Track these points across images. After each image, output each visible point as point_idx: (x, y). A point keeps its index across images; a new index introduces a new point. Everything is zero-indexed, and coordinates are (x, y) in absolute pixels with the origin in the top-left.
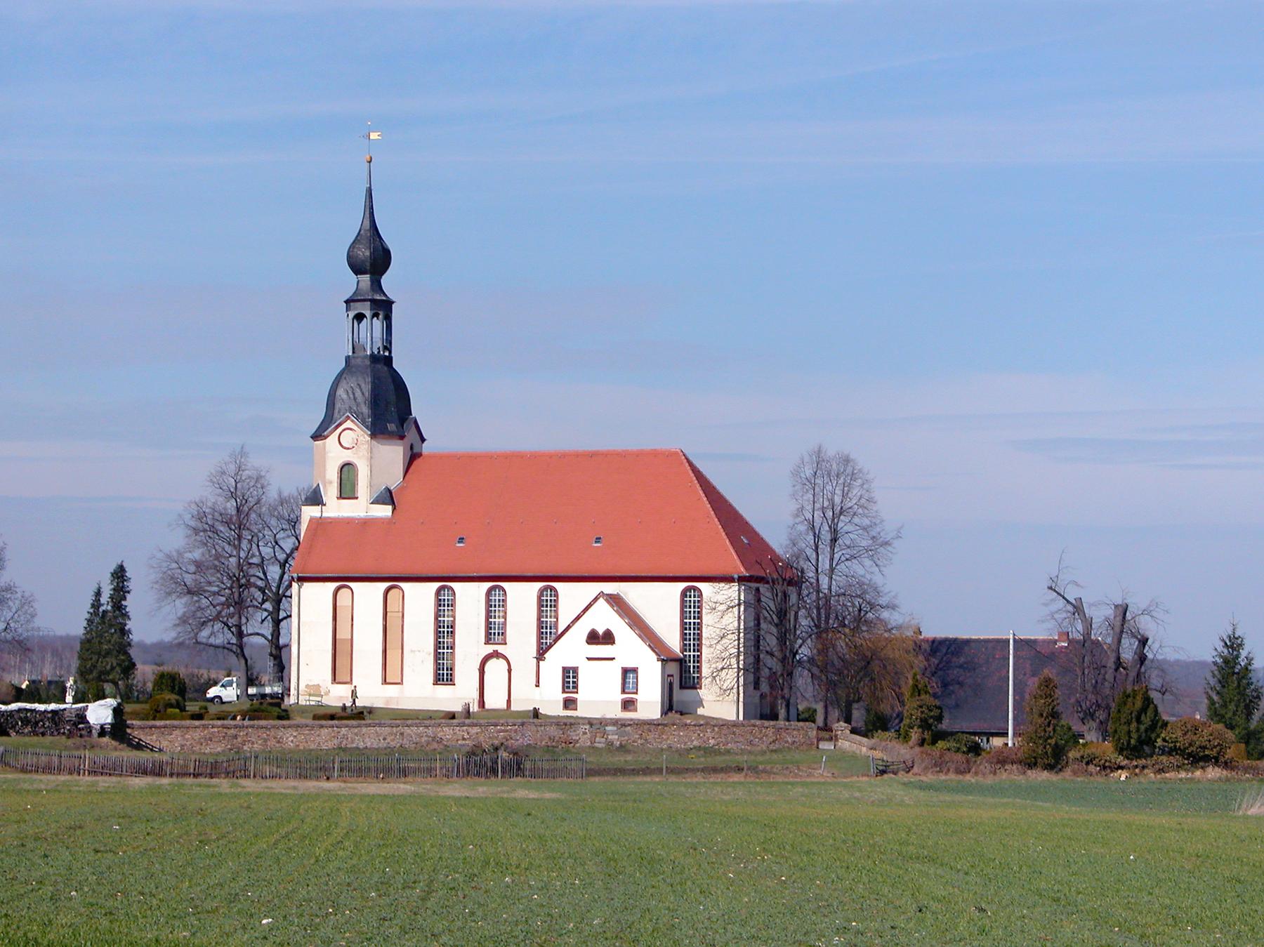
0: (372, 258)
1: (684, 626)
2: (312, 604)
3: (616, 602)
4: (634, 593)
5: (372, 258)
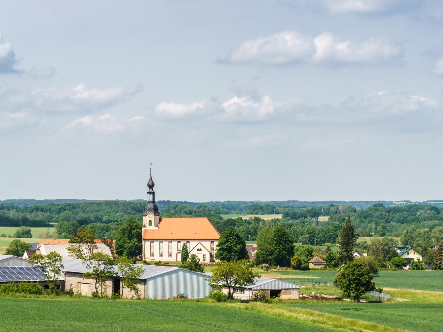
0: (151, 186)
2: (146, 246)
4: (203, 243)
5: (151, 186)
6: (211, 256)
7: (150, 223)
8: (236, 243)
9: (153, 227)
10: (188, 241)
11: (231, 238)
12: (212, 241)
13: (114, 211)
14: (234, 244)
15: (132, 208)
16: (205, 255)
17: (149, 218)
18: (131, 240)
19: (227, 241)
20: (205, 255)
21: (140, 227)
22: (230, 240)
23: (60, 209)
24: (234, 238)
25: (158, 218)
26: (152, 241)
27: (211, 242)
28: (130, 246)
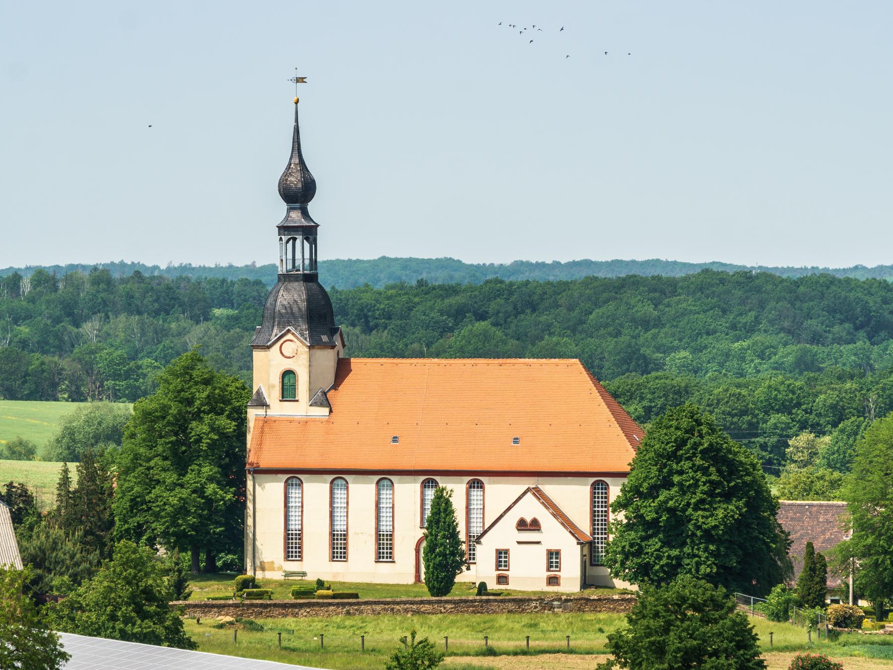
0: (299, 192)
1: (593, 514)
2: (266, 500)
3: (538, 493)
4: (551, 489)
5: (299, 192)
6: (591, 555)
7: (288, 386)
8: (711, 494)
9: (301, 407)
10: (476, 478)
11: (686, 465)
12: (599, 481)
13: (734, 327)
14: (699, 496)
15: (832, 311)
16: (558, 553)
17: (282, 358)
18: (182, 472)
19: (667, 484)
20: (558, 553)
21: (233, 402)
22: (676, 479)
23: (459, 314)
24: (696, 469)
25: (327, 359)
26: (294, 476)
27: (594, 486)
28: (175, 501)
